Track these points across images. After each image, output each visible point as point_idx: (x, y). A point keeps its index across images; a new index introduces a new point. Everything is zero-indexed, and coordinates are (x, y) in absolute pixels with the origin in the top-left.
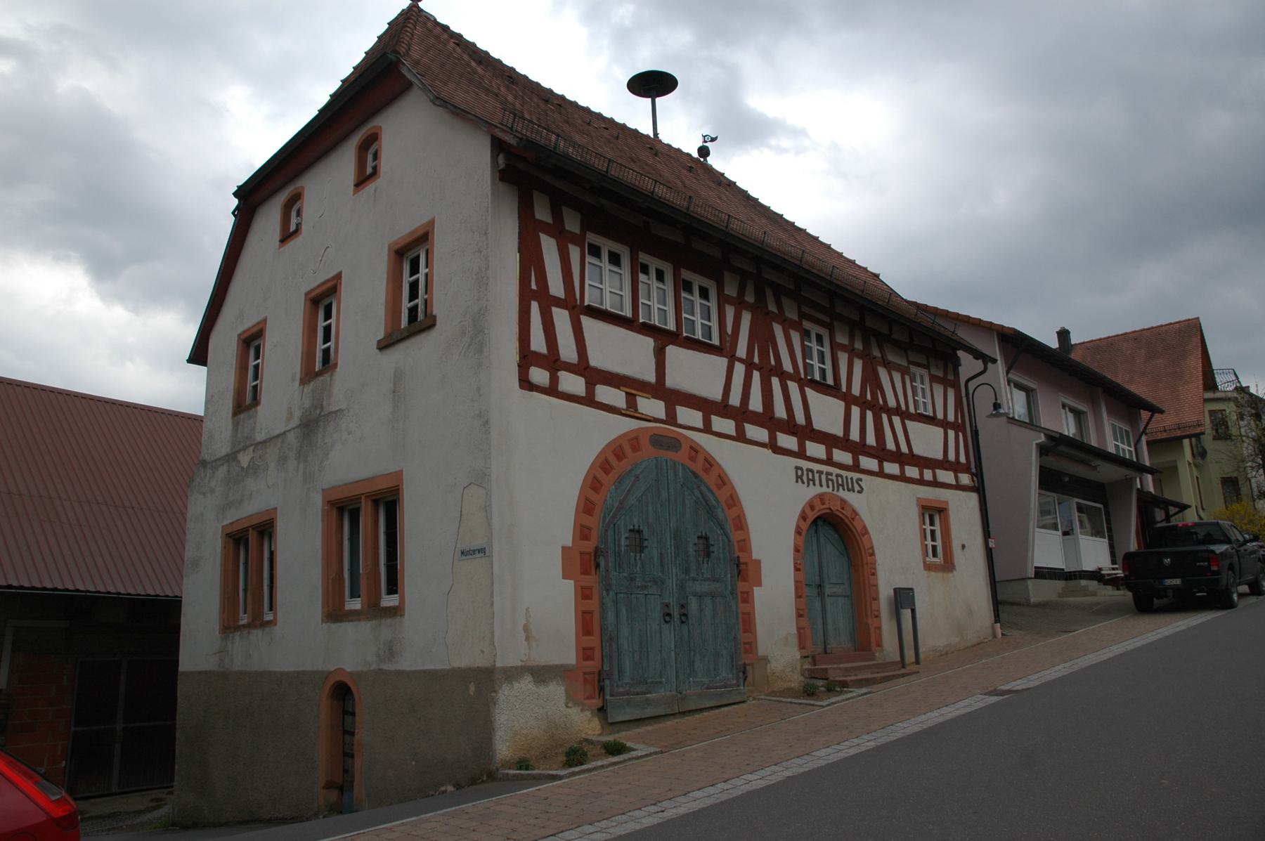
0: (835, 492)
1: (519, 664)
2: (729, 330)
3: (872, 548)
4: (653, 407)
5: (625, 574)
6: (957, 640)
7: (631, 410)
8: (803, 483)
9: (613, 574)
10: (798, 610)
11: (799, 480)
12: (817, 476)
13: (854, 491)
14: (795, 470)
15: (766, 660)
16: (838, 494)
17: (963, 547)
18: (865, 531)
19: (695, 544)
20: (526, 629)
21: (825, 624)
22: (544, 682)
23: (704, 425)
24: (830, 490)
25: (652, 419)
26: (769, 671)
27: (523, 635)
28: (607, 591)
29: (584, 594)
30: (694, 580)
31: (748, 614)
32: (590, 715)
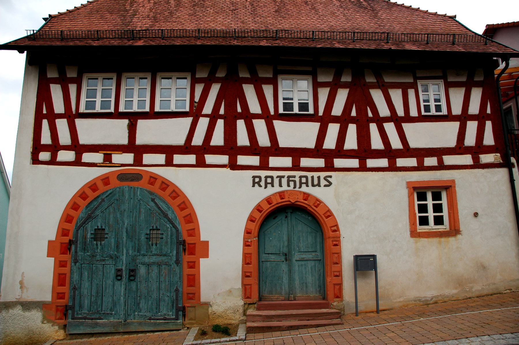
0: (297, 189)
1: (15, 300)
2: (197, 99)
4: (128, 158)
5: (89, 254)
6: (455, 291)
8: (260, 186)
9: (80, 253)
13: (320, 186)
19: (147, 234)
20: (21, 283)
22: (29, 310)
23: (326, 149)
25: (120, 165)
26: (210, 311)
27: (19, 286)
28: (75, 263)
29: (60, 264)
30: (144, 255)
32: (58, 328)
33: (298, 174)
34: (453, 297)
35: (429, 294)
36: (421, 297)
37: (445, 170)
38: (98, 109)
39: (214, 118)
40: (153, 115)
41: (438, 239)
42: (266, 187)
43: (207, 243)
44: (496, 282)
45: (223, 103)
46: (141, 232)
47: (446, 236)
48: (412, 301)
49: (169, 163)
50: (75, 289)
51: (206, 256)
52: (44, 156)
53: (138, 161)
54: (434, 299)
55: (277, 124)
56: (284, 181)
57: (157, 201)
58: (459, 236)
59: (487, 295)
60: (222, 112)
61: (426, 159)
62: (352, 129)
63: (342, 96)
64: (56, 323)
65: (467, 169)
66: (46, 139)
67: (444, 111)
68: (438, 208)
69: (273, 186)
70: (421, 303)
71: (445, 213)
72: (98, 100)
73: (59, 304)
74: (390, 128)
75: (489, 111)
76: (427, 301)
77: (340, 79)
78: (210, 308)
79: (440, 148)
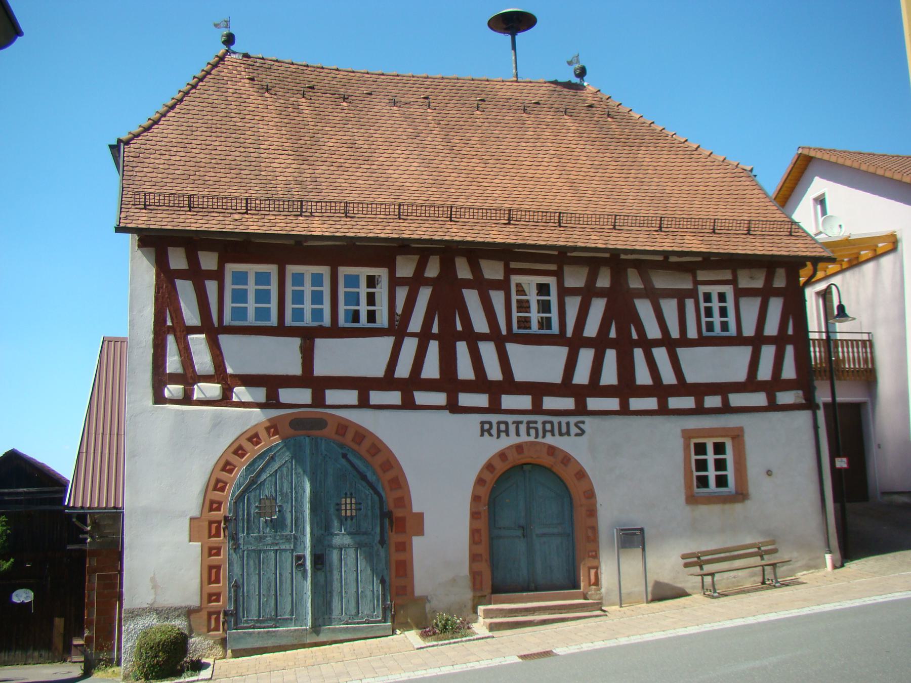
0: (540, 440)
2: (399, 310)
4: (303, 396)
8: (491, 435)
16: (544, 441)
24: (532, 438)
33: (540, 419)
38: (251, 320)
39: (424, 337)
40: (335, 331)
42: (498, 437)
43: (420, 516)
45: (437, 316)
46: (329, 501)
49: (364, 403)
50: (236, 586)
52: (173, 390)
53: (319, 400)
55: (512, 349)
56: (523, 428)
57: (351, 457)
60: (435, 329)
61: (707, 399)
62: (611, 355)
63: (598, 308)
64: (209, 636)
66: (173, 363)
67: (733, 331)
68: (720, 465)
69: (508, 435)
71: (730, 473)
72: (251, 305)
73: (212, 610)
74: (661, 355)
75: (790, 331)
78: (428, 606)
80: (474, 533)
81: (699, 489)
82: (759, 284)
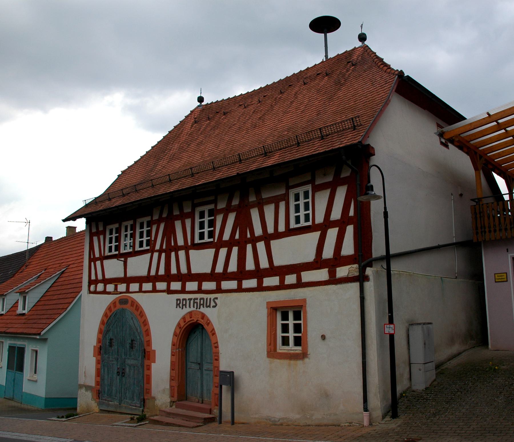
0: (198, 310)
3: (217, 343)
6: (298, 416)
7: (116, 292)
8: (180, 307)
10: (171, 376)
11: (178, 306)
12: (188, 302)
13: (210, 307)
14: (176, 301)
15: (154, 398)
16: (200, 310)
17: (323, 337)
18: (175, 334)
21: (202, 384)
24: (195, 309)
27: (84, 375)
29: (98, 362)
31: (149, 375)
34: (296, 421)
35: (279, 415)
36: (271, 417)
37: (302, 288)
41: (288, 361)
44: (337, 413)
47: (295, 359)
48: (264, 419)
51: (154, 362)
54: (281, 421)
58: (306, 360)
59: (325, 425)
65: (322, 285)
70: (271, 423)
71: (280, 334)
75: (352, 213)
76: (275, 421)
77: (248, 199)
79: (300, 264)
80: (172, 363)
81: (283, 347)
82: (329, 179)
